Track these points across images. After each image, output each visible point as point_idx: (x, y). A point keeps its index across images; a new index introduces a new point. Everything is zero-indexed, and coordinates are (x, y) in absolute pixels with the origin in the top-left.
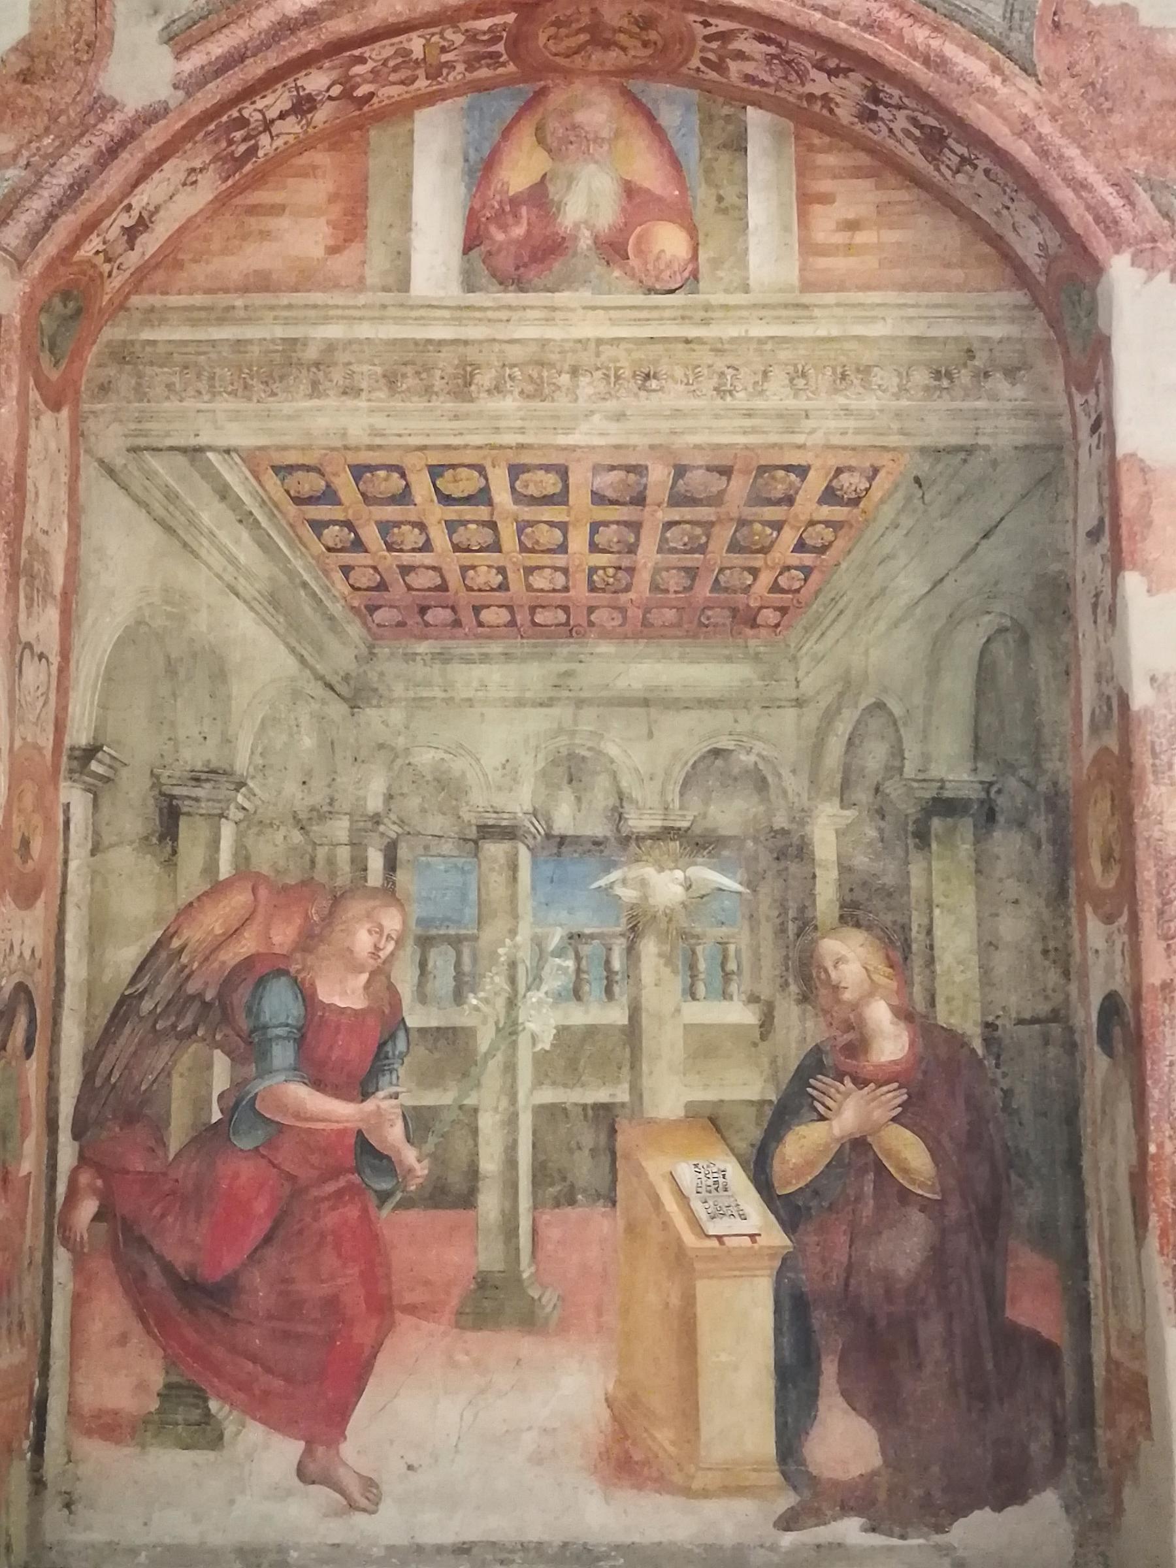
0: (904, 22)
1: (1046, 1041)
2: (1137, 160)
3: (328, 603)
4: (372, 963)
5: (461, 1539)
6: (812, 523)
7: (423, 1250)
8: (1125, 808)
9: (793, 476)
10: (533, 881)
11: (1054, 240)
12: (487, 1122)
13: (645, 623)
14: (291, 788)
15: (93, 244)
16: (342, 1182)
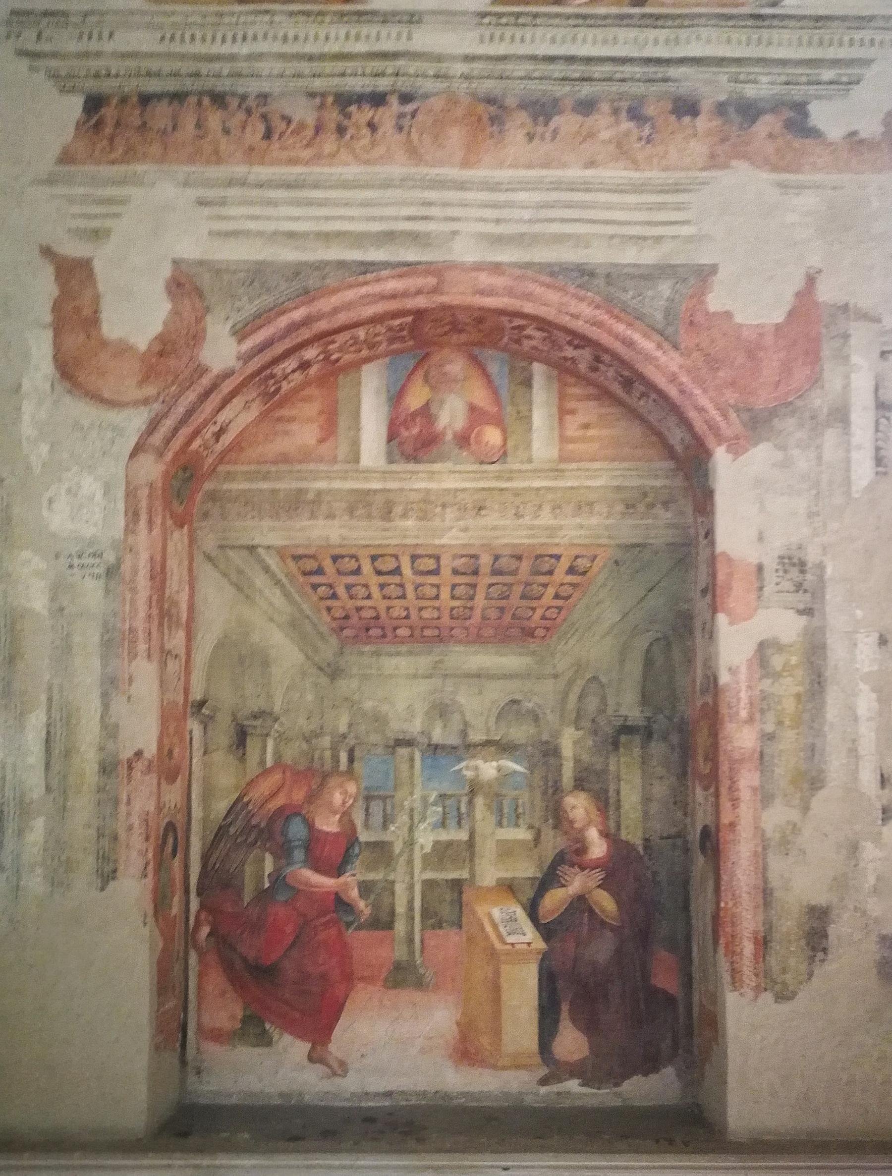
0: (612, 321)
1: (674, 846)
2: (731, 396)
4: (342, 810)
5: (387, 1089)
6: (562, 584)
7: (367, 949)
8: (714, 734)
11: (688, 437)
13: (479, 636)
14: (302, 721)
15: (197, 443)
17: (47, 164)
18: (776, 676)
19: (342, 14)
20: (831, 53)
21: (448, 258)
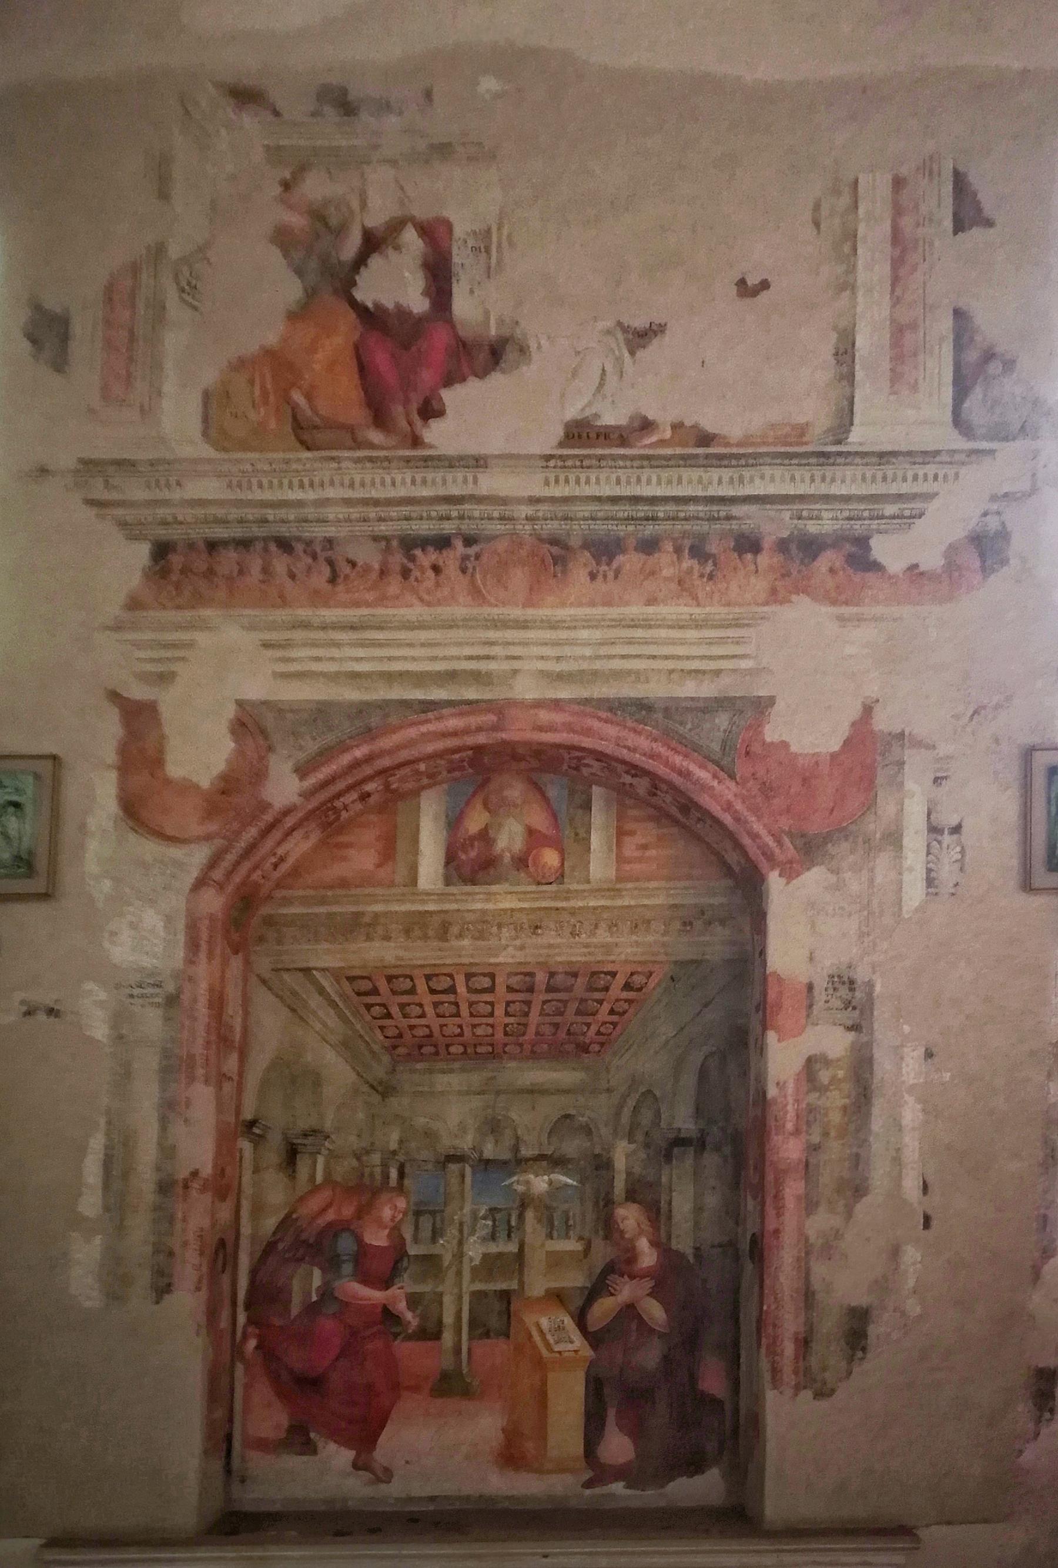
0: (669, 753)
3: (373, 1045)
4: (392, 1224)
9: (609, 977)
10: (472, 1181)
11: (743, 861)
12: (447, 1300)
13: (533, 1052)
14: (353, 1139)
16: (375, 1329)
17: (113, 609)
18: (823, 1090)
19: (408, 460)
20: (894, 489)
21: (510, 695)
